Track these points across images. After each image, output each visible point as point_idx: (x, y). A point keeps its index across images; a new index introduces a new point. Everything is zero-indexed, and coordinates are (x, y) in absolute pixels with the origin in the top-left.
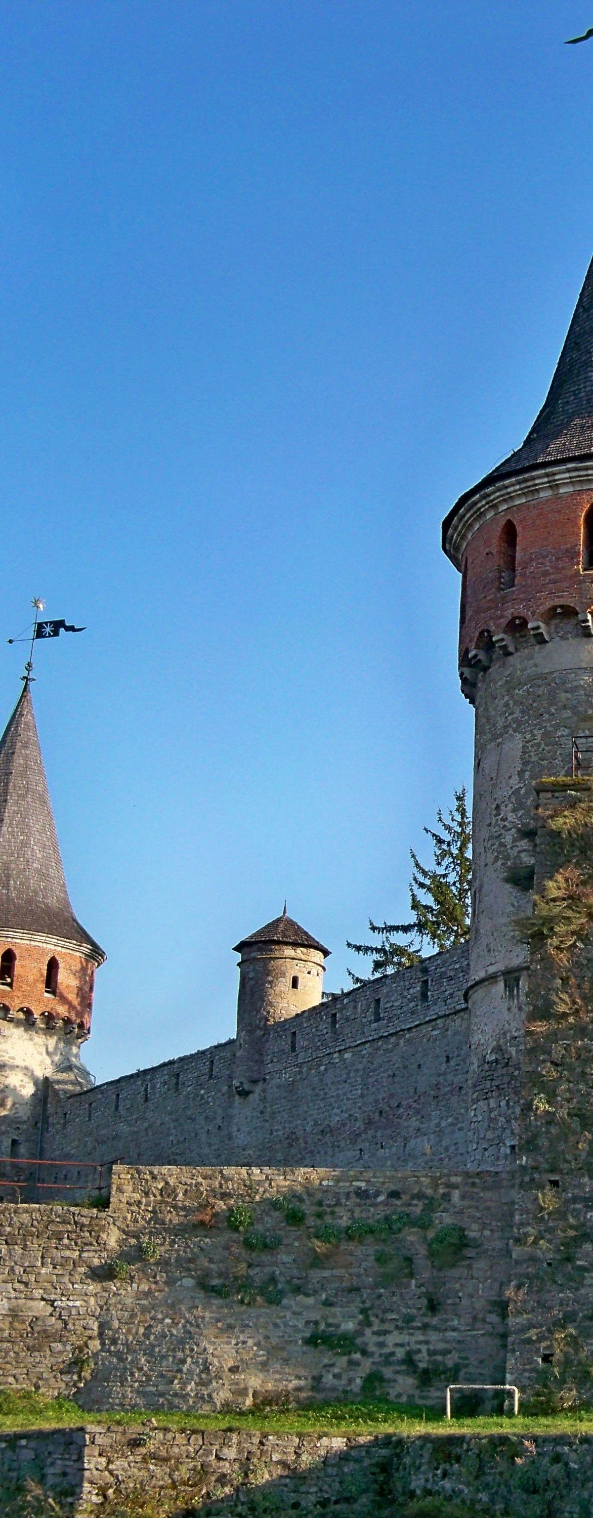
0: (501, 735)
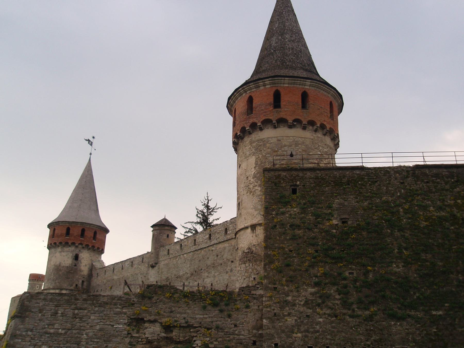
0: (248, 157)
